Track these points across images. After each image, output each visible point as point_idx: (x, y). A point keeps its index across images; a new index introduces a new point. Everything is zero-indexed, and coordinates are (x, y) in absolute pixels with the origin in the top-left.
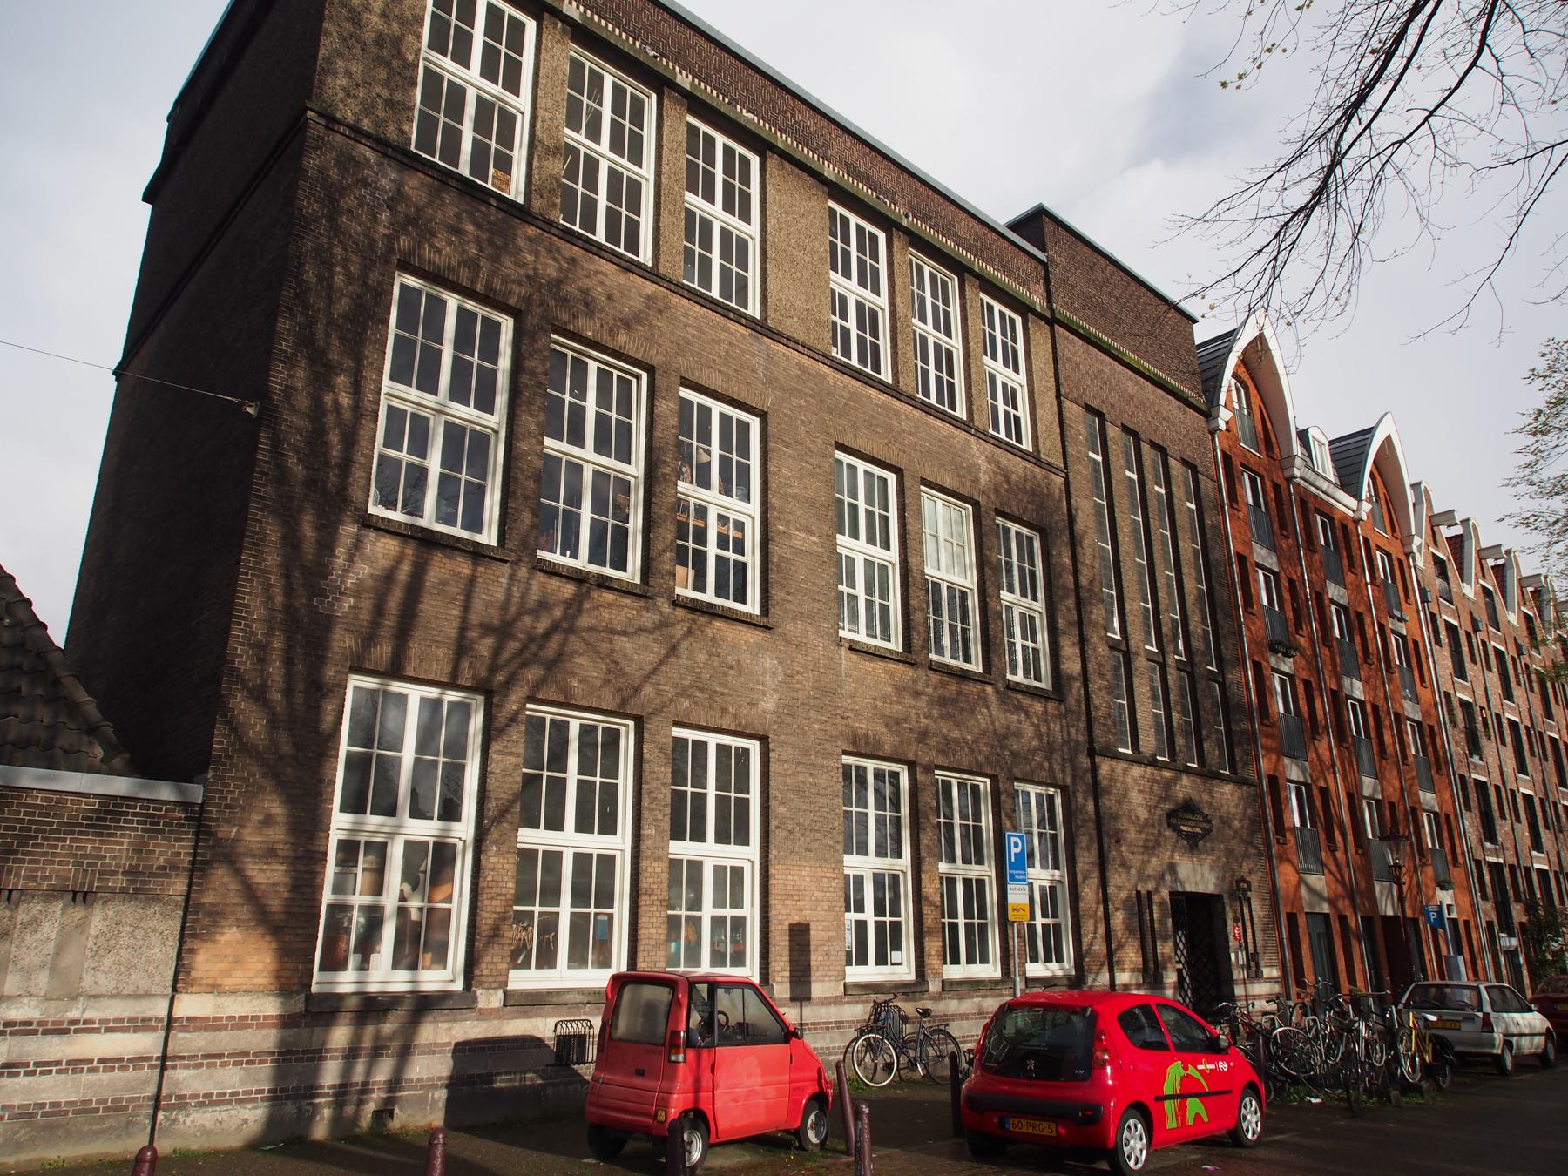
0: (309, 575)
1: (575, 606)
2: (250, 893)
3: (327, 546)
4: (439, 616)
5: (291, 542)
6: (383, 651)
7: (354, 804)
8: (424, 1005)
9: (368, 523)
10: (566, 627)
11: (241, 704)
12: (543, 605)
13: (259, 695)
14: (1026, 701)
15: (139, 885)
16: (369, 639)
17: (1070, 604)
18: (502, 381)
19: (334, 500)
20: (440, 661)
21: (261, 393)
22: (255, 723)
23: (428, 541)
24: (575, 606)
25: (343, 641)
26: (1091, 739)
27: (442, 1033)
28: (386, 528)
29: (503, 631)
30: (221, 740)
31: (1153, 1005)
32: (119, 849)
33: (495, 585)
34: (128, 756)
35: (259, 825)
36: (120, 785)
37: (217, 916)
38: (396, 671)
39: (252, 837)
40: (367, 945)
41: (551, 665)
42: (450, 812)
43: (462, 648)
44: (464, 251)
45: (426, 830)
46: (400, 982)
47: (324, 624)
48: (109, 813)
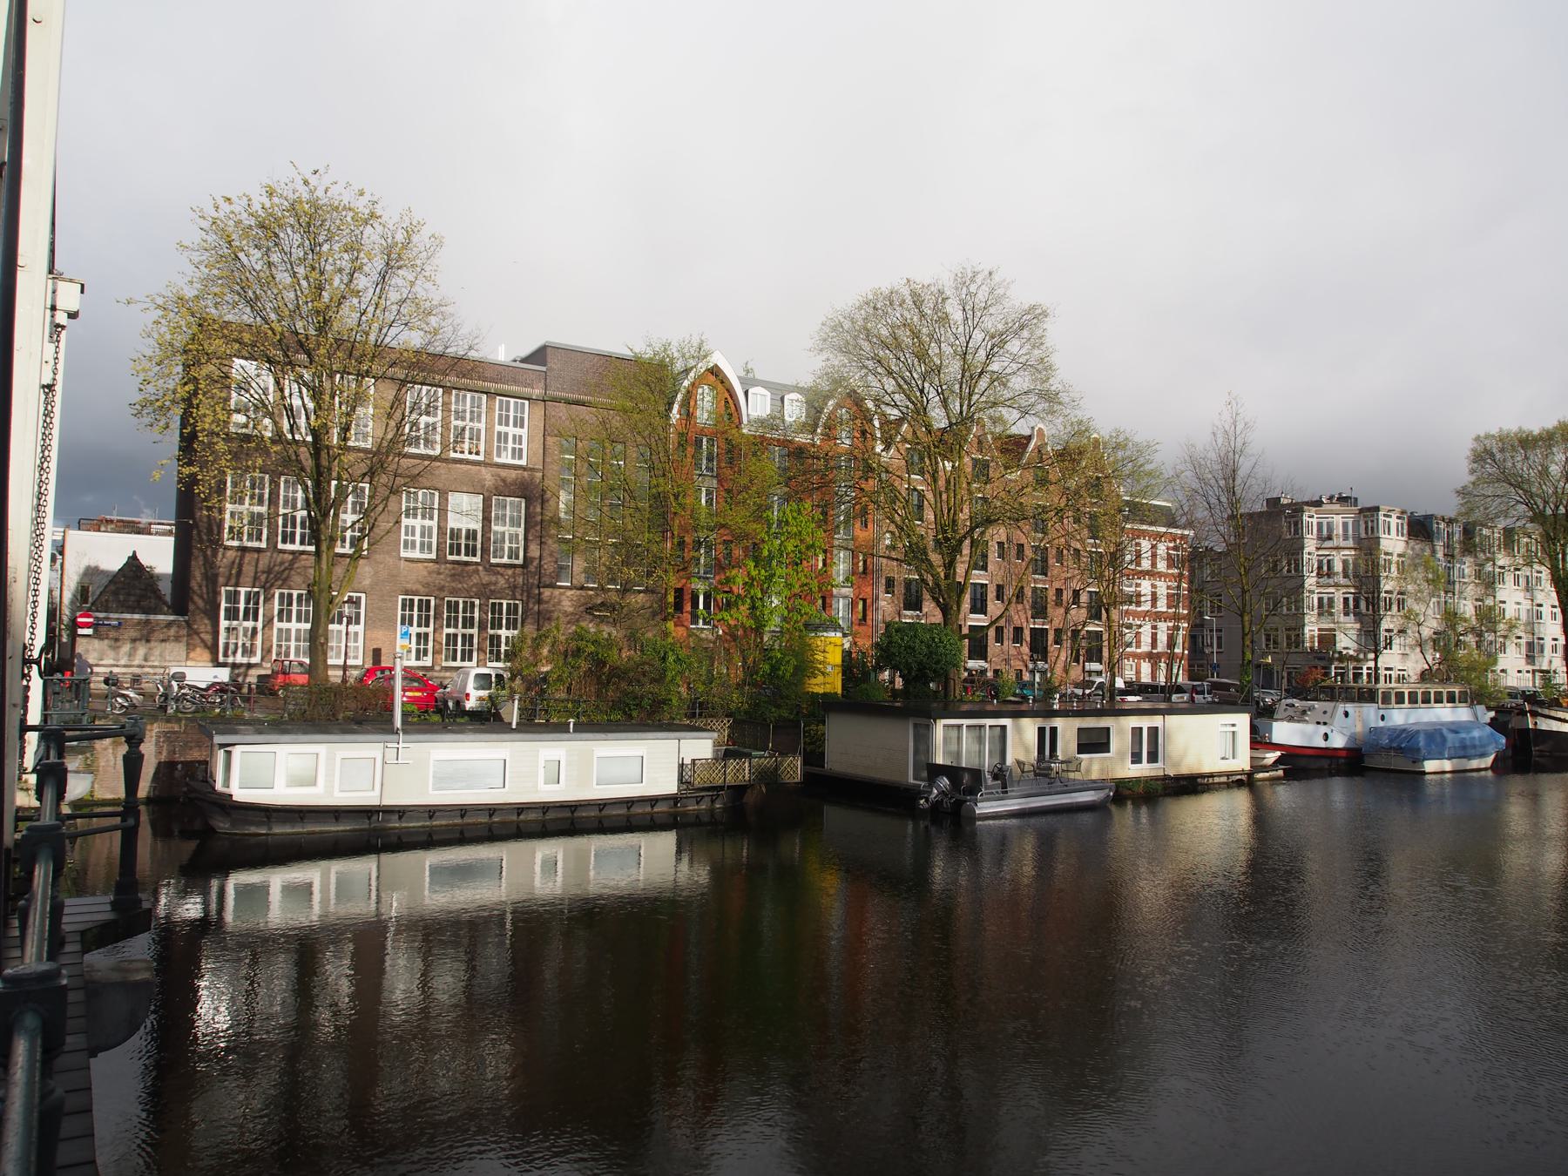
0: (209, 565)
1: (292, 562)
2: (203, 641)
3: (215, 555)
4: (248, 570)
5: (205, 556)
6: (233, 581)
7: (227, 618)
8: (249, 666)
9: (227, 548)
10: (290, 567)
11: (196, 598)
12: (282, 563)
13: (201, 597)
14: (501, 570)
15: (177, 639)
16: (229, 579)
17: (537, 525)
18: (266, 496)
19: (216, 543)
20: (249, 580)
21: (193, 518)
22: (200, 603)
23: (243, 549)
24: (292, 562)
25: (221, 580)
26: (321, 508)
27: (254, 672)
28: (232, 548)
29: (269, 571)
30: (191, 607)
31: (1445, 731)
32: (172, 632)
33: (264, 562)
34: (1562, 796)
35: (203, 625)
36: (172, 618)
37: (195, 647)
38: (237, 585)
39: (202, 628)
40: (235, 653)
41: (285, 580)
42: (256, 619)
43: (256, 578)
44: (771, 658)
45: (250, 624)
46: (245, 660)
47: (216, 576)
48: (169, 625)
